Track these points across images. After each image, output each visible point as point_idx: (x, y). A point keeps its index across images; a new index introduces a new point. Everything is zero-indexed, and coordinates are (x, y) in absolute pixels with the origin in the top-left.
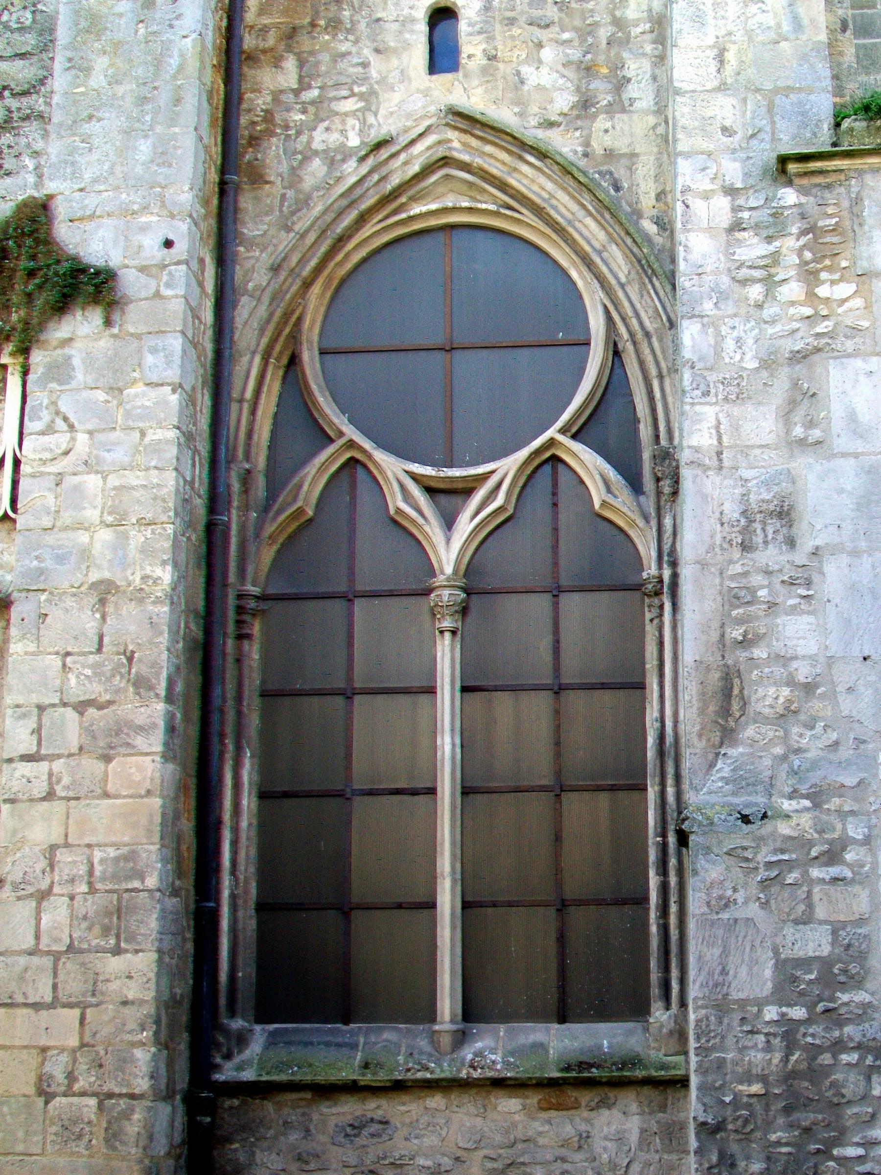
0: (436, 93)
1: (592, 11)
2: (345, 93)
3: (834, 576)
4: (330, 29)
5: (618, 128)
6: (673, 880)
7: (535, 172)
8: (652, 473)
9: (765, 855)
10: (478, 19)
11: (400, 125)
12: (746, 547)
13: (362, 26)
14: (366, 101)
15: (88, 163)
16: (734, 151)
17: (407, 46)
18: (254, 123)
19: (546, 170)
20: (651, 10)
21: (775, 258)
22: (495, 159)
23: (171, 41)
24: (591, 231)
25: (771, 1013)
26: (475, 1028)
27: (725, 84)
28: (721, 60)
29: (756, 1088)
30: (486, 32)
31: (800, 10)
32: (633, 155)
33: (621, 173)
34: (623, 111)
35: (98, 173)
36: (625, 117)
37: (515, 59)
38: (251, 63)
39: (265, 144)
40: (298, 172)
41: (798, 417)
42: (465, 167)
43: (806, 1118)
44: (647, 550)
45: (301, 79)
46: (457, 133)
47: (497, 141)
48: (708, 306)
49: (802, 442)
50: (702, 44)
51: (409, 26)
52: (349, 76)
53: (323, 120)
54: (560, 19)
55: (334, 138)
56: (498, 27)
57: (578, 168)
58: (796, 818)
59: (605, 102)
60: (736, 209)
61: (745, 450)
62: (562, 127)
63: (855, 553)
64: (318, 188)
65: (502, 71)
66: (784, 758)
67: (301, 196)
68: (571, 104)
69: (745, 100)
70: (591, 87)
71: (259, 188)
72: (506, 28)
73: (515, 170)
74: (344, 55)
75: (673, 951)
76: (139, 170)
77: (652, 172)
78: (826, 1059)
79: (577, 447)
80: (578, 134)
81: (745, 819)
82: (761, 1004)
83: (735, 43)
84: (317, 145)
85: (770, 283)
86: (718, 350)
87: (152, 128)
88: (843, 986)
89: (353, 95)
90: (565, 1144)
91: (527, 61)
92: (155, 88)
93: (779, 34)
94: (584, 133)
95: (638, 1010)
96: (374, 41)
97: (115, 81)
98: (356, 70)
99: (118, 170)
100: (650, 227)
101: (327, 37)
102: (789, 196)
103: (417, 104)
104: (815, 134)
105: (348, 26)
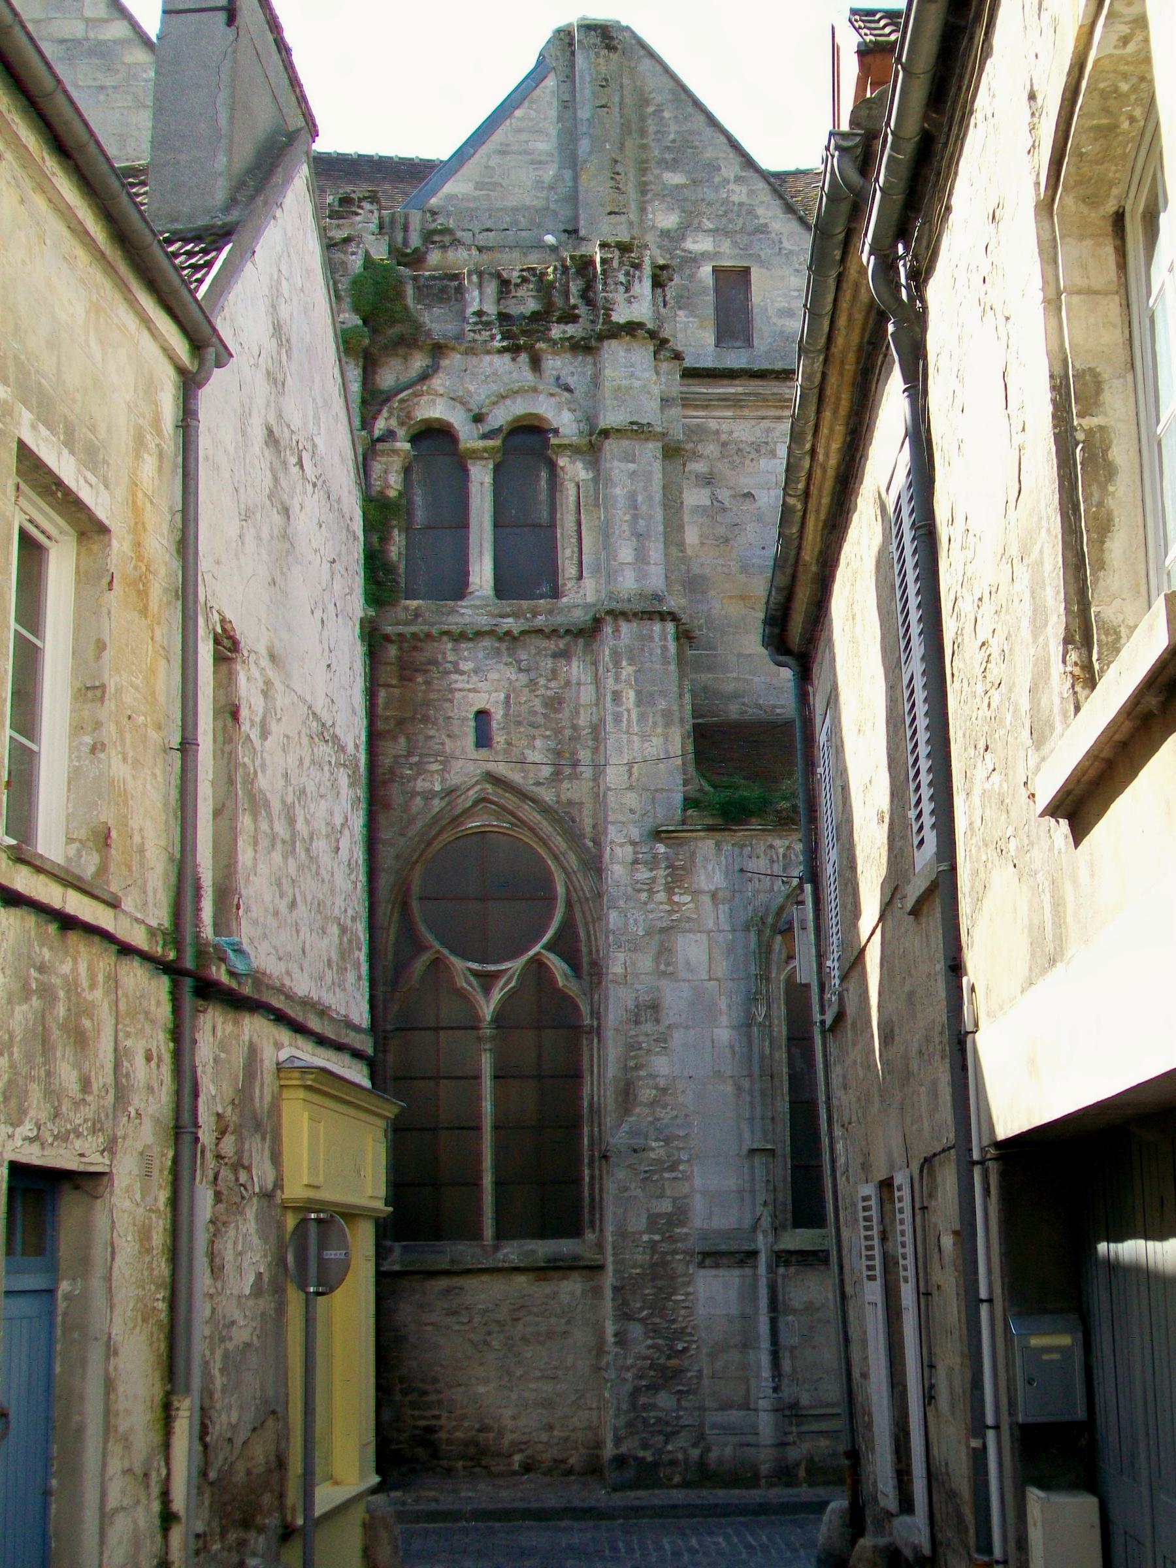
3: (677, 1038)
6: (597, 1172)
8: (589, 970)
12: (637, 1022)
13: (441, 721)
21: (653, 880)
22: (510, 801)
24: (559, 842)
25: (645, 1238)
26: (503, 1242)
33: (575, 813)
43: (659, 1283)
44: (584, 1008)
48: (621, 903)
49: (664, 973)
55: (427, 785)
58: (657, 1150)
60: (636, 853)
61: (637, 975)
66: (651, 1123)
74: (432, 737)
75: (596, 1206)
78: (669, 1258)
79: (552, 956)
81: (635, 1151)
82: (641, 1233)
85: (651, 892)
86: (626, 925)
88: (677, 1226)
90: (547, 1296)
91: (528, 747)
95: (574, 1231)
102: (661, 848)
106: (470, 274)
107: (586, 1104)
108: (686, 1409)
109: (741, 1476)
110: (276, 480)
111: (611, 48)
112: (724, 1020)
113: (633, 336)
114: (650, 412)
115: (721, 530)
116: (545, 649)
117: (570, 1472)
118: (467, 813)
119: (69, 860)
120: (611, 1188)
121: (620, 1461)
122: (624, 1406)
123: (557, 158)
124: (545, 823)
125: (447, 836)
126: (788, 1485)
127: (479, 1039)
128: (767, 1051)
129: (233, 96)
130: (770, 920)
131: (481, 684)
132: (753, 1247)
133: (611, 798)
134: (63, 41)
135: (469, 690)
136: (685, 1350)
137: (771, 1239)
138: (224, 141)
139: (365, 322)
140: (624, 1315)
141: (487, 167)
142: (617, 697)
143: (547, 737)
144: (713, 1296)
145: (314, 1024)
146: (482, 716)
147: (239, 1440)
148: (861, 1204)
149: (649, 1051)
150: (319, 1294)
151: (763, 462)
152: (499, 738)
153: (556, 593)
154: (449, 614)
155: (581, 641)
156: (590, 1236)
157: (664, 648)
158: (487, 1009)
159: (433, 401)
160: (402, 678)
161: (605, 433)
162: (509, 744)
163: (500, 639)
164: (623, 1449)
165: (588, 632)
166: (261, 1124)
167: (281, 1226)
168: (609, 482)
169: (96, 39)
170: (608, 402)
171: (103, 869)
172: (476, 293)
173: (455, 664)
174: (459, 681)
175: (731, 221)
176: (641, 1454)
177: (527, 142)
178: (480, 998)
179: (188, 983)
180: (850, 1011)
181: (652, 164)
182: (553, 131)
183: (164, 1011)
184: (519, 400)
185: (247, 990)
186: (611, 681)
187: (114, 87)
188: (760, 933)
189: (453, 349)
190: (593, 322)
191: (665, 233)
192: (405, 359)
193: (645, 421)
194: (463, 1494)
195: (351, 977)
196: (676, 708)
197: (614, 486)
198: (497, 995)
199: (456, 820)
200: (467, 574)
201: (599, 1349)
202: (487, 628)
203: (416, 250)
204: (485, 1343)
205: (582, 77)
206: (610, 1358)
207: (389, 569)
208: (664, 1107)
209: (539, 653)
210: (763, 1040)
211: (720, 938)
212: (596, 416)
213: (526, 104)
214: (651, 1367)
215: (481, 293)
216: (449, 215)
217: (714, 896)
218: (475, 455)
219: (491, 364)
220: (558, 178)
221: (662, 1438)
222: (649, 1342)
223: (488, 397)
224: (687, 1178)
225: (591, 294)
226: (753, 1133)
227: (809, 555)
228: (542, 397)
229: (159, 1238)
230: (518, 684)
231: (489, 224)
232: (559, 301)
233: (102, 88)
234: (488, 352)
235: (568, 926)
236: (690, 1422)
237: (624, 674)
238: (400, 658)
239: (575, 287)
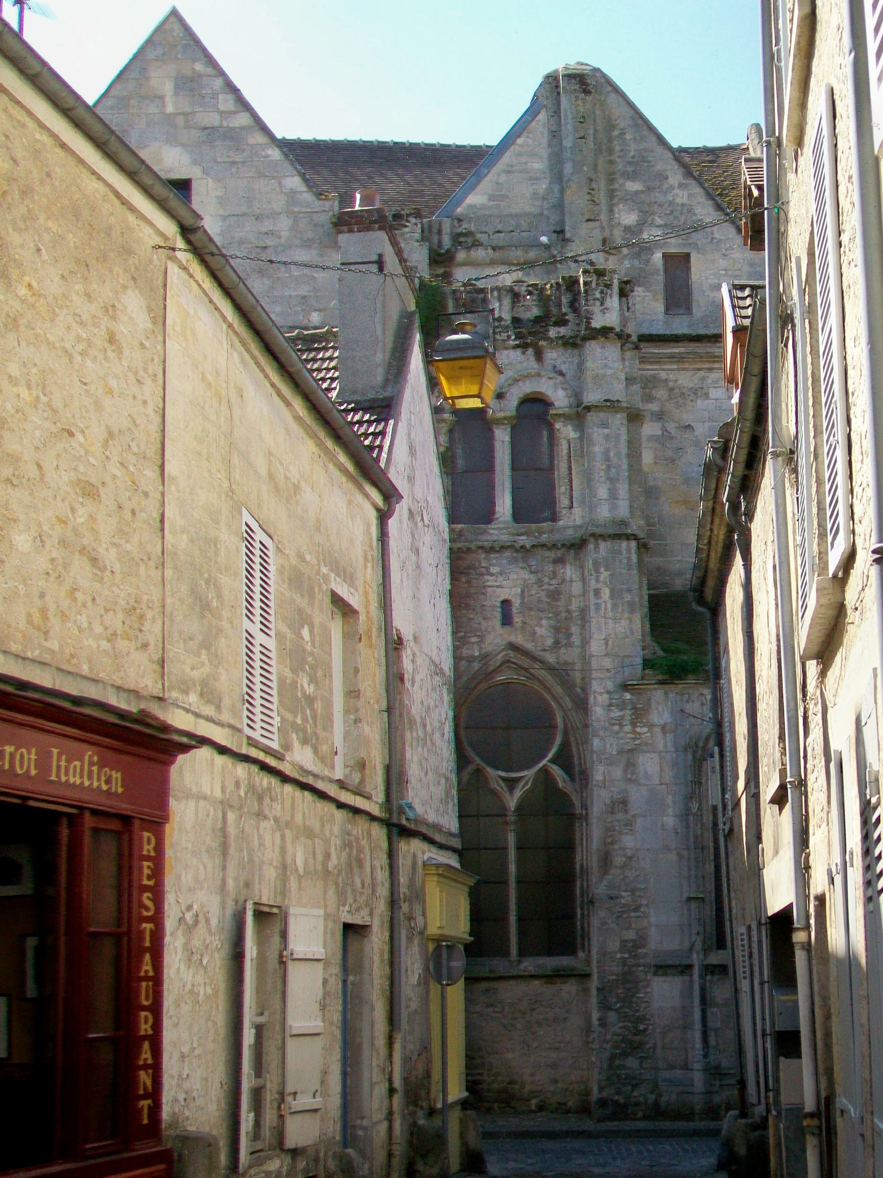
3: (639, 823)
6: (586, 913)
8: (580, 776)
9: (617, 909)
22: (525, 662)
24: (558, 690)
25: (619, 956)
28: (607, 644)
29: (614, 977)
34: (570, 646)
41: (629, 772)
42: (514, 663)
43: (627, 986)
44: (577, 803)
48: (601, 733)
49: (631, 780)
58: (626, 898)
60: (611, 699)
63: (645, 816)
66: (623, 879)
74: (472, 619)
75: (586, 935)
79: (555, 767)
81: (612, 898)
82: (616, 953)
85: (621, 726)
88: (640, 948)
91: (536, 626)
95: (573, 952)
100: (579, 690)
102: (628, 696)
103: (498, 640)
106: (492, 291)
107: (578, 867)
108: (645, 1069)
109: (682, 1113)
110: (413, 536)
111: (587, 92)
112: (670, 811)
113: (606, 338)
114: (618, 391)
115: (670, 453)
116: (548, 557)
117: (568, 1111)
118: (497, 670)
119: (346, 776)
120: (595, 922)
121: (603, 1103)
122: (605, 1066)
123: (548, 176)
124: (550, 678)
125: (483, 686)
126: (714, 1119)
127: (507, 823)
128: (699, 832)
129: (384, 316)
130: (701, 745)
131: (506, 582)
132: (688, 962)
133: (594, 664)
134: (206, 128)
135: (497, 587)
136: (645, 1030)
137: (701, 956)
138: (380, 345)
140: (605, 1006)
141: (497, 183)
142: (597, 592)
143: (549, 618)
144: (663, 995)
145: (438, 838)
146: (506, 603)
147: (414, 1058)
148: (740, 937)
149: (620, 832)
150: (448, 985)
151: (699, 402)
152: (517, 619)
153: (554, 518)
154: (481, 534)
156: (581, 954)
157: (629, 559)
158: (512, 802)
161: (588, 409)
163: (517, 551)
164: (605, 1094)
165: (578, 546)
166: (418, 896)
167: (427, 948)
168: (591, 443)
169: (228, 127)
171: (362, 781)
173: (487, 569)
174: (490, 580)
175: (676, 218)
176: (616, 1098)
177: (526, 163)
178: (506, 795)
179: (395, 830)
180: (736, 829)
181: (618, 175)
182: (545, 153)
183: (385, 845)
184: (527, 382)
185: (412, 826)
186: (593, 582)
187: (243, 163)
188: (694, 752)
190: (578, 325)
191: (627, 229)
193: (615, 399)
194: (500, 1123)
195: (450, 806)
196: (637, 600)
197: (594, 445)
198: (518, 793)
199: (489, 675)
200: (493, 504)
201: (588, 1030)
202: (509, 544)
203: (448, 251)
204: (513, 1026)
205: (566, 116)
206: (595, 1035)
208: (631, 869)
210: (697, 824)
211: (668, 756)
212: (581, 393)
213: (525, 134)
214: (622, 1041)
216: (470, 220)
217: (663, 727)
218: (499, 422)
219: (508, 357)
220: (549, 190)
221: (629, 1088)
222: (621, 1024)
223: (506, 380)
224: (646, 916)
225: (577, 305)
226: (690, 886)
227: (713, 564)
228: (544, 380)
229: (386, 956)
230: (530, 582)
231: (500, 227)
232: (554, 310)
233: (234, 163)
234: (506, 348)
235: (565, 746)
236: (648, 1077)
237: (602, 577)
239: (565, 300)
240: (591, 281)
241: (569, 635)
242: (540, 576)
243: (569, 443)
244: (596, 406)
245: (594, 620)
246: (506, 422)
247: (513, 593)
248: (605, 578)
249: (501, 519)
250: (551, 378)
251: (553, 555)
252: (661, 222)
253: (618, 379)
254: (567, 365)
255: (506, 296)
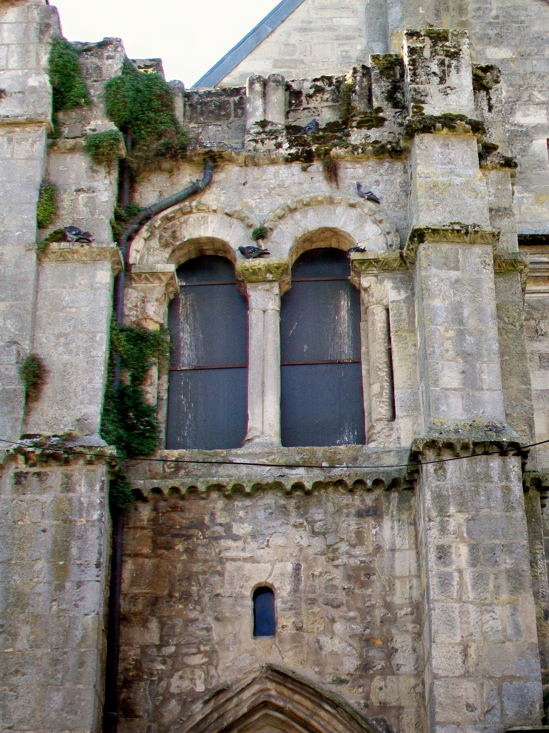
0: (259, 653)
1: (370, 596)
2: (194, 650)
4: (183, 600)
5: (389, 687)
7: (330, 716)
10: (289, 598)
11: (234, 677)
14: (209, 657)
15: (15, 708)
16: (475, 723)
17: (239, 616)
18: (127, 670)
19: (339, 717)
20: (411, 598)
22: (301, 705)
23: (76, 618)
27: (468, 672)
28: (465, 654)
30: (294, 609)
31: (519, 619)
32: (400, 708)
33: (392, 721)
34: (393, 674)
35: (23, 716)
36: (394, 678)
37: (315, 630)
38: (125, 623)
39: (135, 686)
40: (159, 710)
42: (280, 710)
45: (161, 638)
46: (274, 684)
47: (303, 692)
50: (452, 641)
51: (240, 601)
52: (197, 638)
53: (178, 670)
54: (347, 601)
55: (186, 684)
56: (303, 605)
57: (361, 716)
59: (380, 667)
62: (349, 684)
64: (174, 723)
65: (306, 639)
67: (162, 728)
68: (355, 667)
69: (482, 685)
70: (370, 654)
71: (132, 721)
72: (309, 606)
73: (316, 714)
76: (53, 715)
77: (413, 721)
80: (361, 690)
83: (474, 641)
84: (173, 689)
87: (62, 684)
89: (199, 652)
91: (324, 632)
92: (65, 653)
93: (505, 636)
94: (366, 689)
96: (215, 611)
97: (35, 645)
98: (201, 633)
99: (38, 714)
101: (181, 606)
103: (246, 661)
104: (530, 712)
105: (196, 599)
123: (364, 32)
131: (259, 550)
133: (440, 691)
135: (245, 560)
139: (123, 128)
142: (443, 553)
143: (351, 619)
146: (263, 592)
152: (285, 621)
153: (362, 439)
155: (395, 495)
157: (507, 490)
159: (205, 219)
160: (156, 546)
161: (419, 235)
162: (299, 629)
163: (288, 494)
165: (405, 483)
170: (421, 201)
172: (259, 102)
173: (228, 527)
177: (331, 19)
184: (311, 214)
186: (434, 532)
189: (231, 160)
192: (171, 172)
196: (526, 566)
197: (432, 296)
202: (271, 480)
207: (145, 412)
209: (339, 511)
215: (265, 103)
218: (256, 277)
228: (339, 210)
230: (310, 551)
232: (359, 105)
234: (273, 162)
237: (452, 525)
238: (154, 521)
239: (379, 89)
240: (422, 49)
241: (391, 653)
242: (331, 539)
243: (388, 310)
244: (435, 231)
245: (437, 605)
246: (270, 276)
247: (276, 572)
248: (460, 526)
249: (257, 440)
250: (352, 206)
251: (357, 503)
252: (543, 99)
253: (473, 190)
254: (381, 186)
255: (276, 89)
